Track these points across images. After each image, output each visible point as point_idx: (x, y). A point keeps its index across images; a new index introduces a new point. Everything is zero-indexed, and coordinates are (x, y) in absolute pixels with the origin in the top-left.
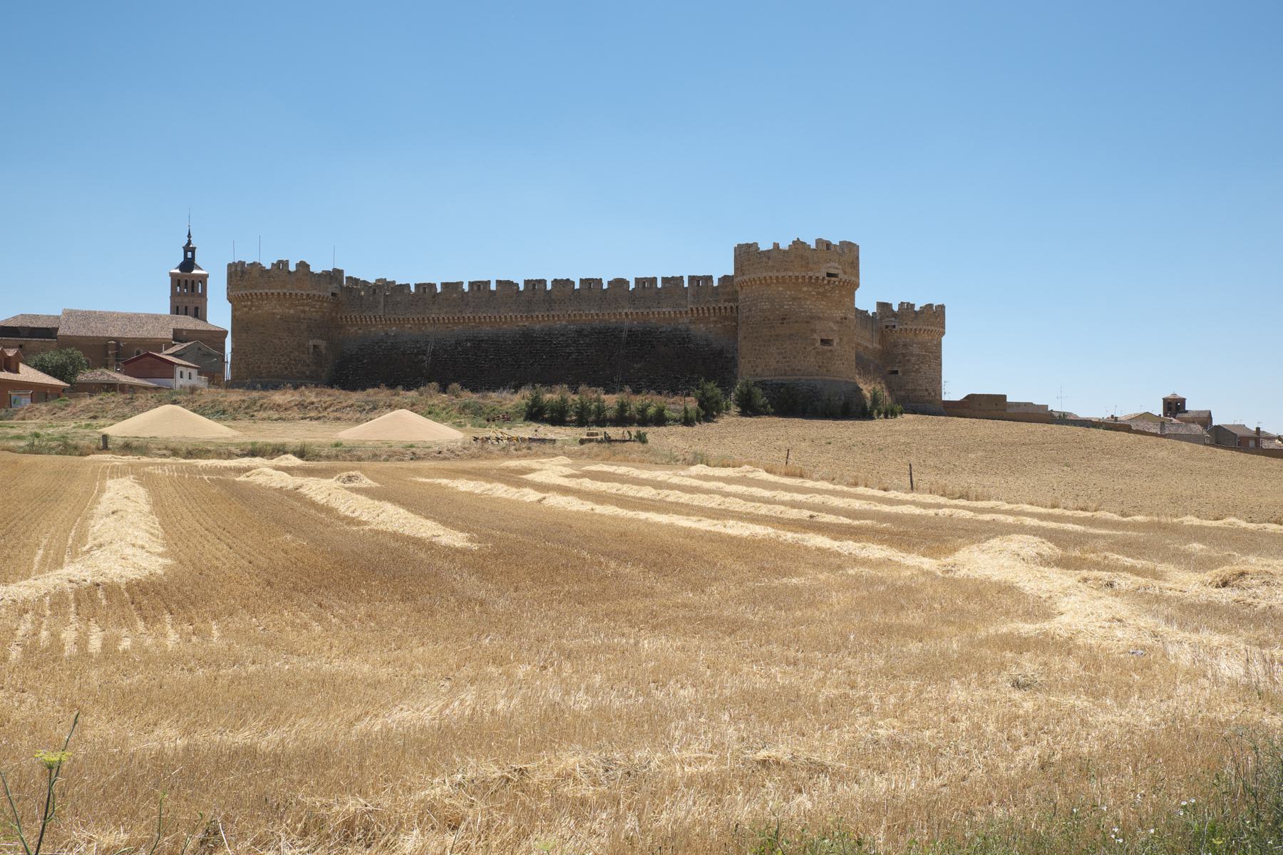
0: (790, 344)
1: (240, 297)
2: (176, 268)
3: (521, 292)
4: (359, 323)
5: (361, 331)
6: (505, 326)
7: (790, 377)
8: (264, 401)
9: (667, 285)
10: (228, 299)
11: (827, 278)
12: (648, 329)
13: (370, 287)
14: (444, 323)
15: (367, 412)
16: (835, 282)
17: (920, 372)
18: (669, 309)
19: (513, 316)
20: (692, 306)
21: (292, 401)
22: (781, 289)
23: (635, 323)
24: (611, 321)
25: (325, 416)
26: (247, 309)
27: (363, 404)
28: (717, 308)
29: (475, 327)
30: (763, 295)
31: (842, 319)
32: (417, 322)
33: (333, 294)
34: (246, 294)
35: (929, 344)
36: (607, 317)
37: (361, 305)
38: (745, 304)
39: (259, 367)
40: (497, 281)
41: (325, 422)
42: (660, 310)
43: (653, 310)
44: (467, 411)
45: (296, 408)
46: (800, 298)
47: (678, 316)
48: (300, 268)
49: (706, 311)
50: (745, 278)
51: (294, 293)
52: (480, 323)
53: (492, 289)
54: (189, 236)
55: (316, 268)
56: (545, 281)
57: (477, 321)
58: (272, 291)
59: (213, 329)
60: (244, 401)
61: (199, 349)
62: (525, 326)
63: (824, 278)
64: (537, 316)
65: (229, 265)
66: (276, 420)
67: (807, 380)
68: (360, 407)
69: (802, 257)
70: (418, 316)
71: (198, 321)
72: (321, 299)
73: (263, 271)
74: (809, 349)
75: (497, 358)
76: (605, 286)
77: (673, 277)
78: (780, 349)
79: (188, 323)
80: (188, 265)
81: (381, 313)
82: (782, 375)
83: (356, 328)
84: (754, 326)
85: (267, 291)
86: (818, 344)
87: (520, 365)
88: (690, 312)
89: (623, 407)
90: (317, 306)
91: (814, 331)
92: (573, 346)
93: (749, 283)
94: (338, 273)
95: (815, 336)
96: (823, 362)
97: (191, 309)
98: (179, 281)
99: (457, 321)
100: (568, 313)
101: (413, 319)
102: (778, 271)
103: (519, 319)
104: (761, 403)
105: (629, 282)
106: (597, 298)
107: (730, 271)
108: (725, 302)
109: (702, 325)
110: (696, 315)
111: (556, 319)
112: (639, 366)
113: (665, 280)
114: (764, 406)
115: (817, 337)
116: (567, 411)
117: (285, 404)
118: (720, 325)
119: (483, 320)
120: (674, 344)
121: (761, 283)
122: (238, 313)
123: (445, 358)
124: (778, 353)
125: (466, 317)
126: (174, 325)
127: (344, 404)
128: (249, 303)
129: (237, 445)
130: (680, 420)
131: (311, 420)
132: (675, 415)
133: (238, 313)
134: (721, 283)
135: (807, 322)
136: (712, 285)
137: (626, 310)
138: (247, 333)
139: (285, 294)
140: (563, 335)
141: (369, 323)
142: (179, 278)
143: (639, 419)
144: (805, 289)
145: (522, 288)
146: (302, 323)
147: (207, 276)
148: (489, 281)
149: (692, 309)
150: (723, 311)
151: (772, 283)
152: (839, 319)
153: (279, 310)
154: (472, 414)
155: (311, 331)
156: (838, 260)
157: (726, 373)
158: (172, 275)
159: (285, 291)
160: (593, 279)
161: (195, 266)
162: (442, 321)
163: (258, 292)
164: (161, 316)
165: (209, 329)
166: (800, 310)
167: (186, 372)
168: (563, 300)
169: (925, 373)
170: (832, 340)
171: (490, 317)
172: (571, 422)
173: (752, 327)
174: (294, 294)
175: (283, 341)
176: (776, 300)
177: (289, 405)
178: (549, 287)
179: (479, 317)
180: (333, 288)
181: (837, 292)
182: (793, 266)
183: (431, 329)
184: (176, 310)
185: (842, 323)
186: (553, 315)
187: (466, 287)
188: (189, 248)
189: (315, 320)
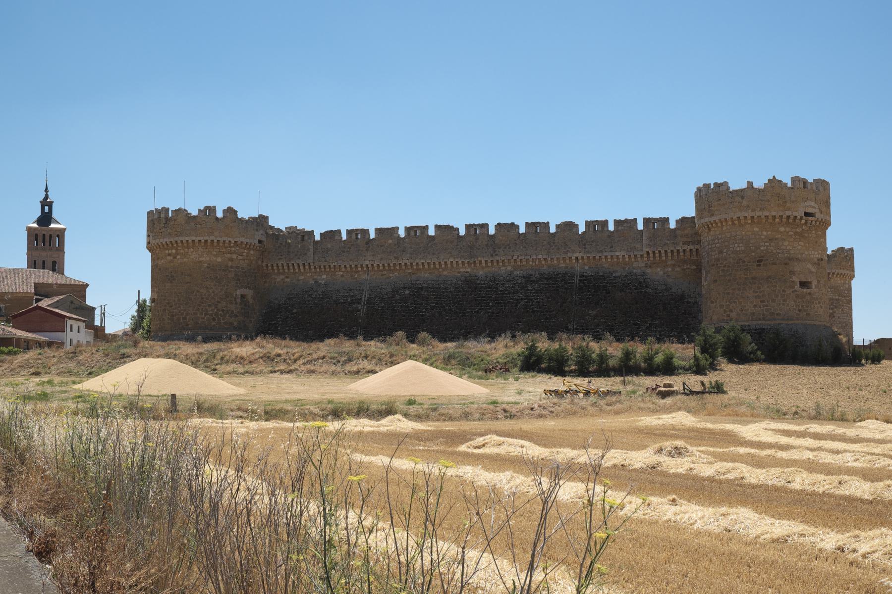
0: (768, 287)
1: (163, 245)
2: (34, 223)
3: (461, 237)
4: (286, 271)
5: (288, 280)
6: (445, 273)
7: (769, 322)
8: (225, 353)
9: (620, 228)
10: (147, 248)
11: (804, 217)
12: (601, 274)
13: (298, 234)
14: (379, 270)
15: (342, 365)
16: (812, 221)
17: (834, 316)
18: (623, 253)
19: (454, 262)
20: (647, 250)
21: (256, 352)
22: (756, 229)
23: (586, 268)
24: (560, 266)
25: (297, 369)
26: (172, 258)
27: (336, 355)
28: (675, 251)
29: (413, 274)
30: (735, 236)
31: (818, 260)
32: (349, 269)
33: (260, 242)
34: (171, 242)
35: (842, 288)
36: (555, 262)
37: (289, 252)
38: (713, 246)
39: (185, 318)
40: (376, 229)
41: (298, 376)
42: (613, 254)
43: (605, 254)
44: (453, 362)
45: (261, 360)
46: (776, 239)
47: (633, 260)
48: (228, 214)
49: (663, 255)
50: (714, 218)
51: (221, 240)
52: (418, 269)
53: (430, 234)
54: (46, 190)
55: (244, 213)
56: (487, 225)
57: (415, 267)
58: (199, 238)
59: (74, 283)
60: (201, 354)
61: (72, 302)
62: (467, 272)
63: (802, 217)
64: (480, 262)
65: (150, 213)
66: (243, 374)
67: (787, 324)
68: (333, 358)
69: (778, 195)
70: (351, 263)
71: (57, 275)
72: (248, 246)
73: (189, 218)
74: (788, 291)
75: (439, 306)
76: (318, 238)
77: (626, 219)
78: (757, 292)
79: (47, 277)
80: (45, 218)
81: (311, 261)
82: (760, 319)
83: (282, 277)
84: (726, 269)
85: (194, 238)
86: (797, 286)
87: (464, 313)
88: (645, 255)
89: (627, 355)
90: (244, 254)
91: (792, 273)
92: (521, 293)
93: (719, 224)
94: (263, 220)
95: (794, 278)
96: (802, 306)
97: (49, 263)
98: (37, 235)
99: (392, 268)
100: (514, 258)
101: (345, 266)
102: (753, 210)
103: (461, 266)
104: (750, 348)
105: (578, 225)
106: (545, 243)
107: (690, 211)
108: (684, 244)
109: (659, 269)
110: (652, 259)
111: (501, 264)
112: (595, 312)
113: (617, 223)
114: (753, 352)
115: (796, 279)
116: (567, 360)
117: (249, 357)
118: (678, 269)
119: (421, 267)
120: (631, 289)
121: (733, 224)
122: (160, 262)
123: (383, 307)
124: (756, 297)
125: (403, 264)
126: (33, 279)
127: (315, 356)
128: (174, 251)
129: (317, 403)
130: (690, 368)
131: (282, 373)
132: (683, 363)
133: (160, 262)
134: (679, 225)
135: (786, 264)
136: (519, 232)
137: (577, 255)
138: (171, 282)
139: (212, 241)
140: (509, 281)
141: (297, 271)
142: (36, 232)
143: (645, 369)
144: (782, 229)
145: (462, 232)
146: (230, 271)
147: (64, 230)
148: (427, 226)
149: (648, 253)
150: (682, 254)
151: (746, 223)
152: (816, 260)
153: (205, 258)
154: (459, 364)
155: (239, 280)
156: (814, 199)
157: (690, 319)
158: (29, 229)
159: (213, 238)
160: (539, 223)
161: (52, 220)
162: (376, 268)
163: (184, 239)
164: (20, 270)
165: (65, 282)
166: (778, 251)
167: (76, 324)
168: (509, 245)
169: (839, 317)
170: (810, 283)
171: (428, 263)
172: (571, 372)
173: (723, 270)
174: (222, 241)
175: (211, 291)
176: (752, 242)
177: (252, 358)
178: (492, 231)
179: (417, 263)
180: (259, 235)
181: (814, 232)
182: (770, 205)
183: (364, 276)
184: (33, 264)
185: (819, 264)
186: (498, 261)
187: (402, 233)
188: (46, 203)
189: (243, 269)
